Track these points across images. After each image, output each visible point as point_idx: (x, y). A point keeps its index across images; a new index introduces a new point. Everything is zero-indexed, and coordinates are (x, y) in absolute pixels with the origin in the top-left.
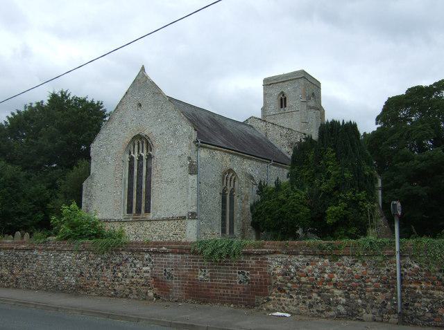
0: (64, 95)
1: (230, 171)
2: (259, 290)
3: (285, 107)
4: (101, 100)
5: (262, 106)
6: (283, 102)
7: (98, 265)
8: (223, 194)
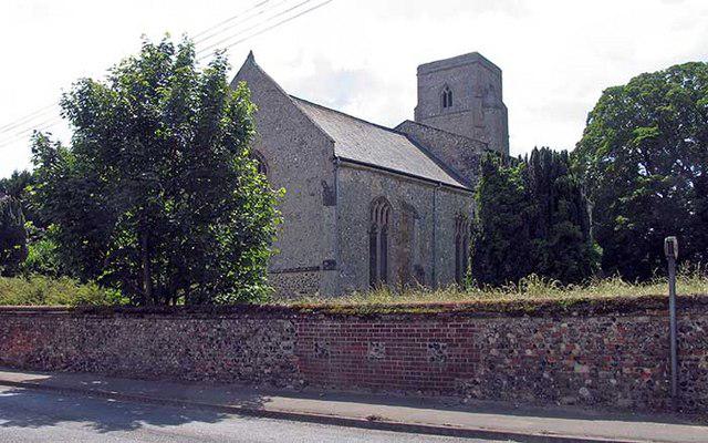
0: (546, 152)
1: (382, 199)
2: (460, 370)
3: (451, 105)
4: (563, 149)
5: (415, 104)
6: (447, 99)
7: (212, 339)
8: (372, 233)
